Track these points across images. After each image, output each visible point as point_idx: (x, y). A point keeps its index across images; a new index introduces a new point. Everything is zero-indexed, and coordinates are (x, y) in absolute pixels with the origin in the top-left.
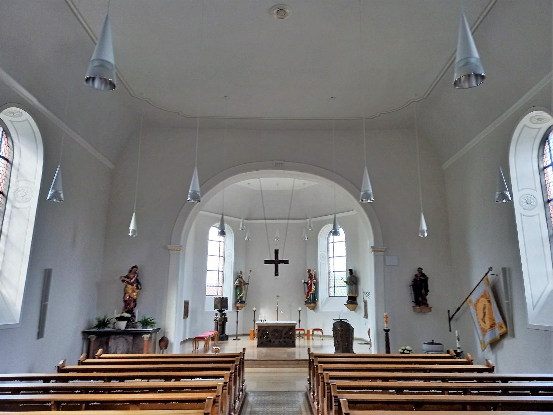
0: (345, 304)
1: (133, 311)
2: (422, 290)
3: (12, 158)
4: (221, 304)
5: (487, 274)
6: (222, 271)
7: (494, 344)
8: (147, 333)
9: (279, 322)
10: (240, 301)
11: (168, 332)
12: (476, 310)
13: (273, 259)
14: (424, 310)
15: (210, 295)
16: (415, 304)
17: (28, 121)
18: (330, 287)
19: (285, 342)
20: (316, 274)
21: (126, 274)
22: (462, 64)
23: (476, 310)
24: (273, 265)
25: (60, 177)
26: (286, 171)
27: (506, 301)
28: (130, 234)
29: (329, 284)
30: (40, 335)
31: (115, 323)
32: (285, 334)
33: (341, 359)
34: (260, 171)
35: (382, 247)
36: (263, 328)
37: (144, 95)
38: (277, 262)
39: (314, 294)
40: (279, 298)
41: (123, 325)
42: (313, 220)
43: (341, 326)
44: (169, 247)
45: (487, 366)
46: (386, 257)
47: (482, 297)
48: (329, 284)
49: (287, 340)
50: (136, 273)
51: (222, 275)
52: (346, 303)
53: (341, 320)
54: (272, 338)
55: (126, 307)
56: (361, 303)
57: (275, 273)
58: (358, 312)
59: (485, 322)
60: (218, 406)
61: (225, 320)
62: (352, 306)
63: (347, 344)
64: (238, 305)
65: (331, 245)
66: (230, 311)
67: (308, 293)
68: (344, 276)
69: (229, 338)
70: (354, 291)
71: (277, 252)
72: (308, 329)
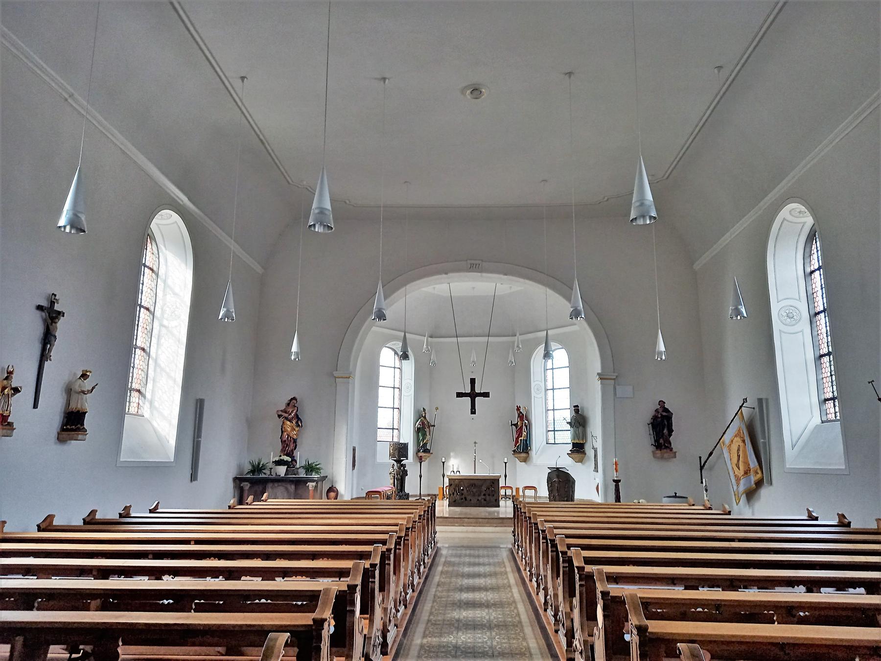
1: (293, 453)
3: (158, 267)
4: (399, 452)
5: (741, 407)
6: (398, 408)
7: (751, 495)
8: (313, 481)
10: (423, 449)
11: (336, 481)
13: (468, 390)
14: (666, 455)
15: (383, 440)
16: (655, 448)
17: (177, 224)
18: (549, 431)
19: (485, 500)
21: (283, 408)
22: (638, 204)
26: (484, 274)
27: (763, 440)
28: (293, 358)
29: (547, 426)
30: (193, 477)
31: (271, 469)
34: (450, 275)
37: (305, 183)
38: (473, 395)
39: (526, 441)
41: (282, 470)
42: (521, 338)
43: (558, 477)
44: (336, 374)
45: (723, 511)
46: (617, 387)
47: (736, 436)
48: (547, 426)
49: (488, 498)
50: (295, 407)
51: (398, 413)
52: (570, 452)
53: (557, 468)
55: (283, 450)
56: (590, 452)
58: (587, 464)
59: (739, 469)
60: (415, 531)
61: (405, 473)
62: (576, 455)
64: (420, 454)
66: (410, 461)
67: (517, 438)
68: (568, 415)
70: (581, 435)
71: (473, 381)
72: (517, 487)
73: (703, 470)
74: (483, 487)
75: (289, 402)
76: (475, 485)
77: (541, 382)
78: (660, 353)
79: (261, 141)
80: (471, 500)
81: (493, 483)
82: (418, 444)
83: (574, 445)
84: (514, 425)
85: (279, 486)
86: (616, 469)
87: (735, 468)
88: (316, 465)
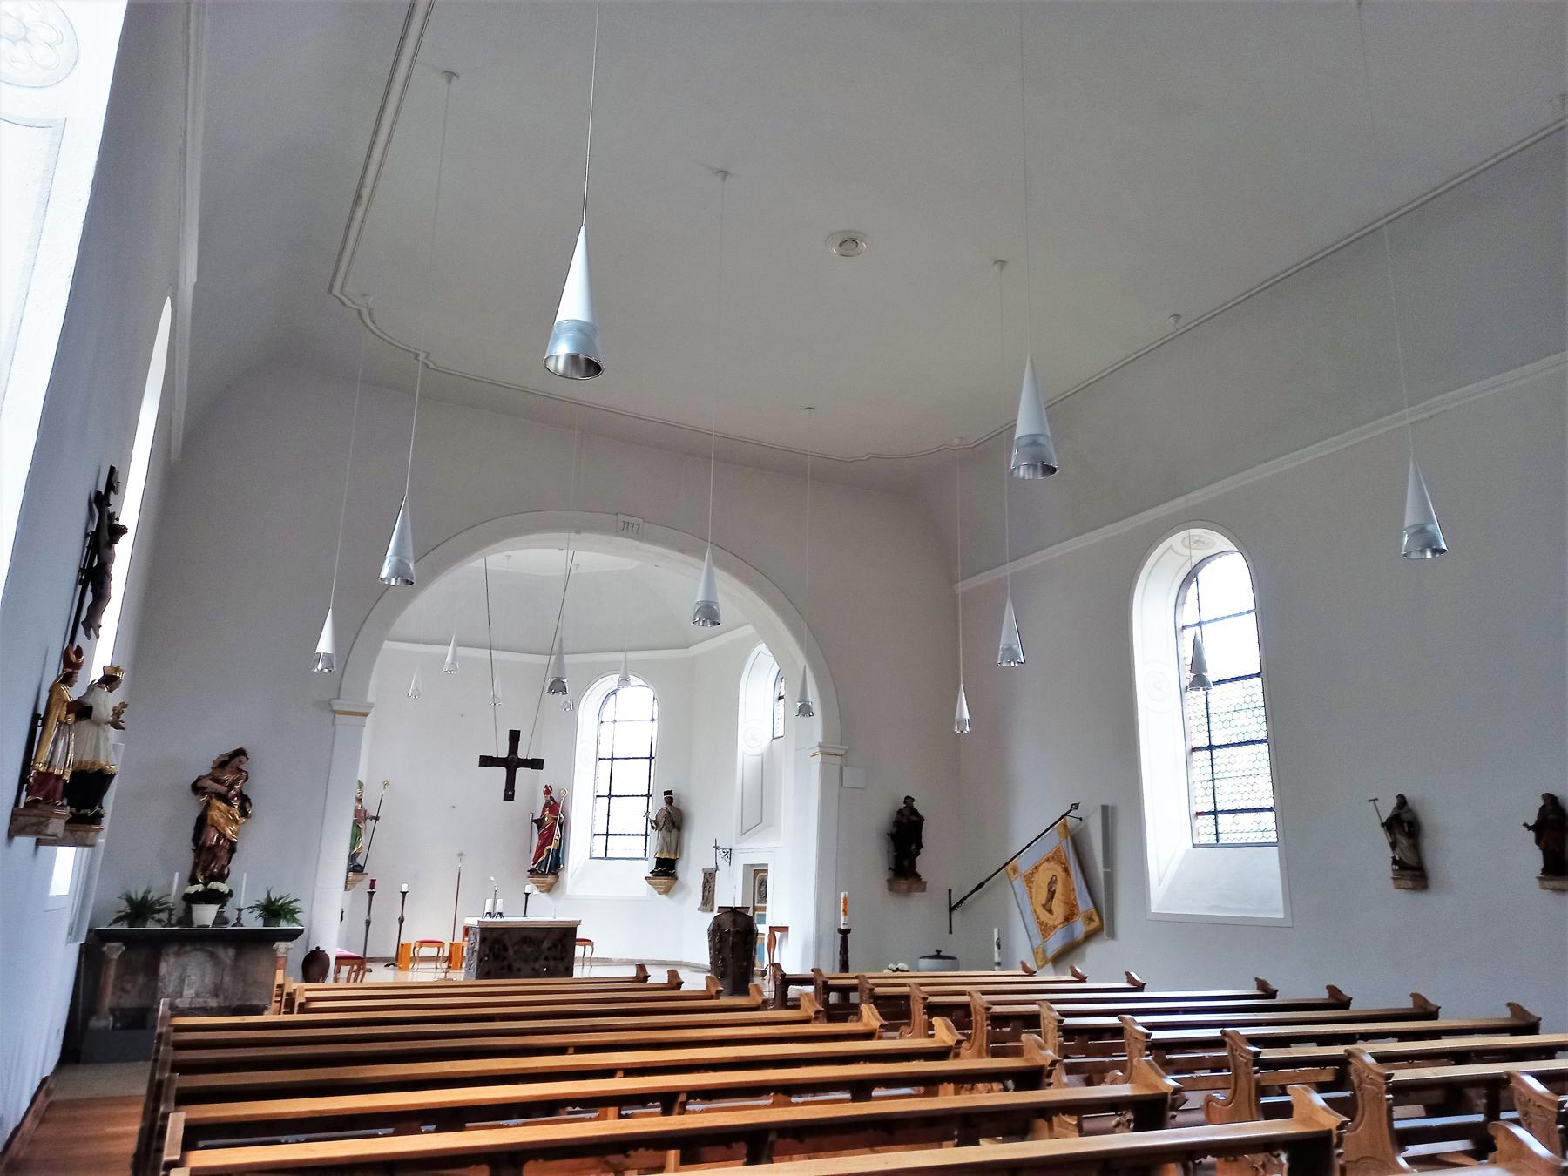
2: (911, 846)
5: (1066, 814)
12: (1030, 888)
13: (503, 753)
23: (1030, 888)
25: (408, 504)
32: (549, 949)
33: (569, 1022)
34: (584, 535)
35: (837, 746)
39: (558, 851)
40: (463, 857)
50: (241, 771)
52: (650, 875)
57: (506, 791)
62: (664, 880)
63: (745, 964)
70: (673, 845)
73: (266, 896)
75: (227, 759)
78: (961, 722)
79: (358, 197)
83: (660, 862)
85: (195, 950)
86: (844, 911)
87: (1040, 911)
88: (290, 902)
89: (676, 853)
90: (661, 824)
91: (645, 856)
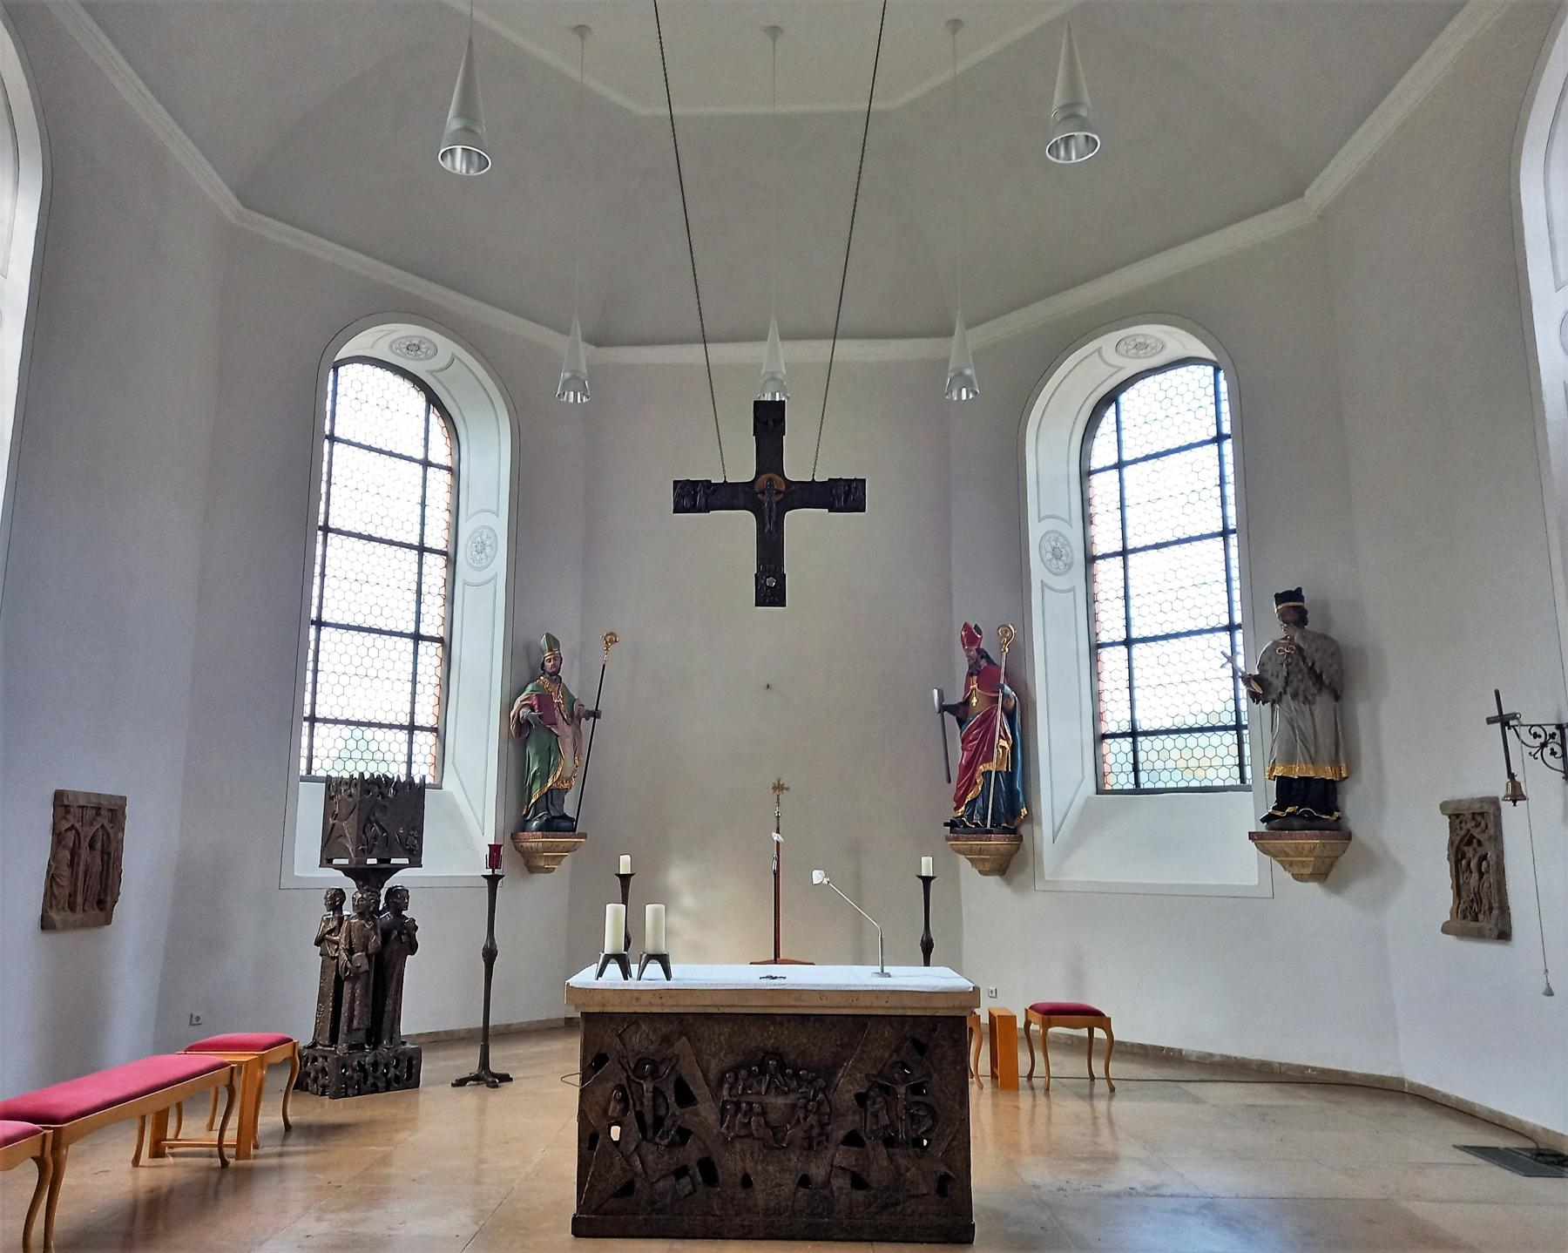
0: (1252, 836)
4: (365, 824)
6: (440, 640)
9: (796, 977)
18: (1105, 736)
20: (1020, 649)
24: (745, 521)
36: (639, 1040)
39: (1010, 776)
48: (1097, 717)
49: (880, 1163)
52: (1263, 827)
54: (726, 1143)
62: (1309, 841)
65: (1103, 487)
67: (969, 767)
69: (429, 1067)
70: (1325, 741)
74: (841, 1079)
76: (782, 1066)
77: (1069, 523)
80: (746, 1182)
81: (920, 1048)
82: (524, 791)
83: (1288, 789)
84: (951, 709)
89: (1335, 763)
90: (1278, 684)
91: (1242, 777)
